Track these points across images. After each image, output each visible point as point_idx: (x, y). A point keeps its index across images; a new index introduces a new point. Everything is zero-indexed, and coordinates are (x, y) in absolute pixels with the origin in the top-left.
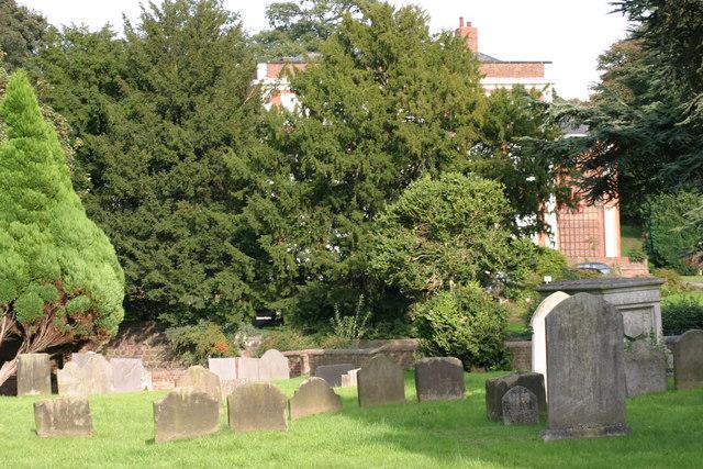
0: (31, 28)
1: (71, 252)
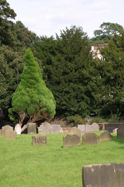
0: (32, 37)
1: (42, 96)
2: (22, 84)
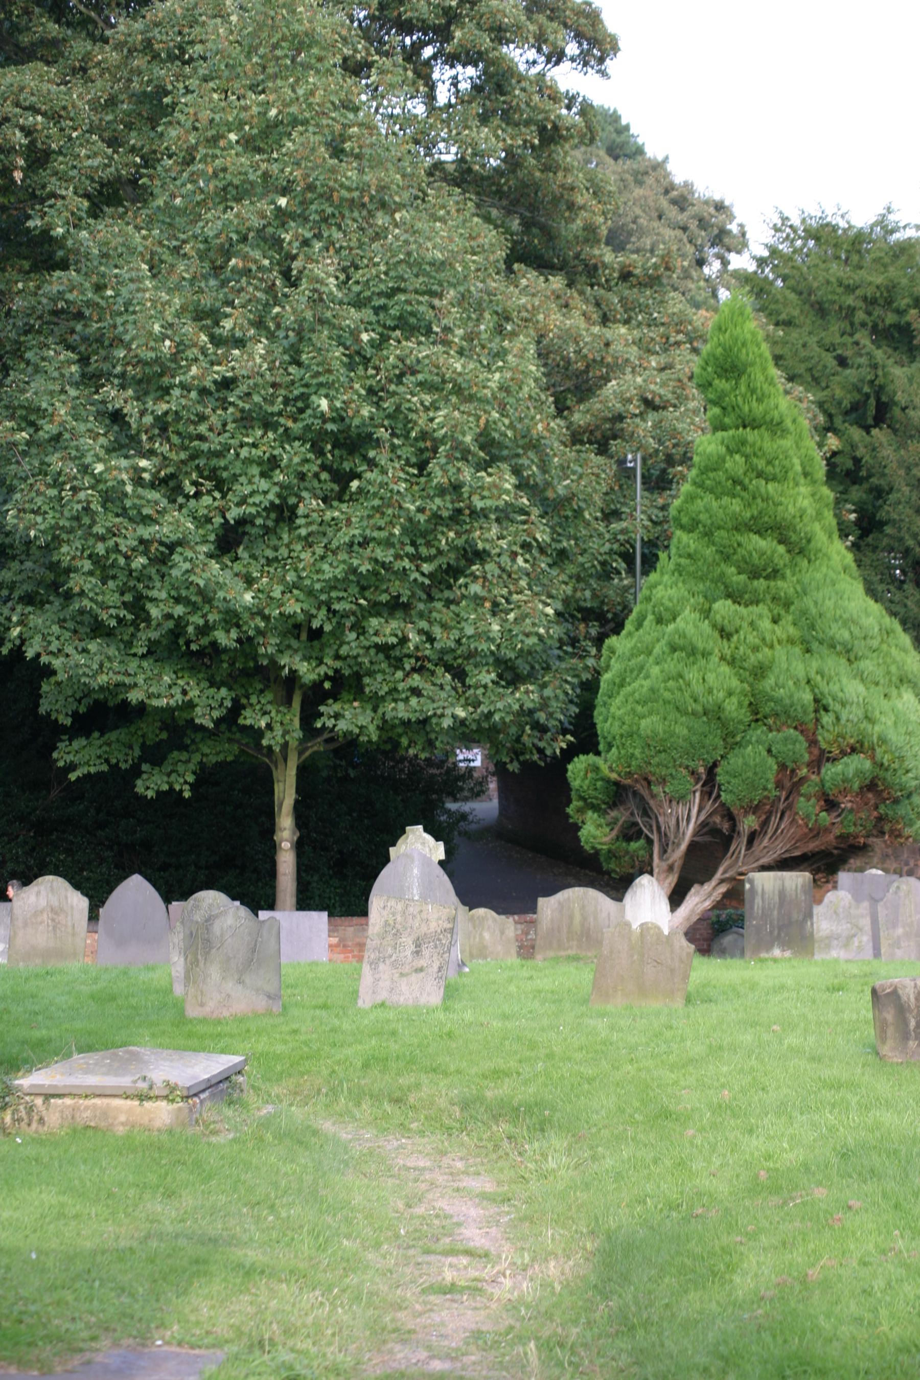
0: (703, 223)
1: (834, 664)
2: (679, 570)
